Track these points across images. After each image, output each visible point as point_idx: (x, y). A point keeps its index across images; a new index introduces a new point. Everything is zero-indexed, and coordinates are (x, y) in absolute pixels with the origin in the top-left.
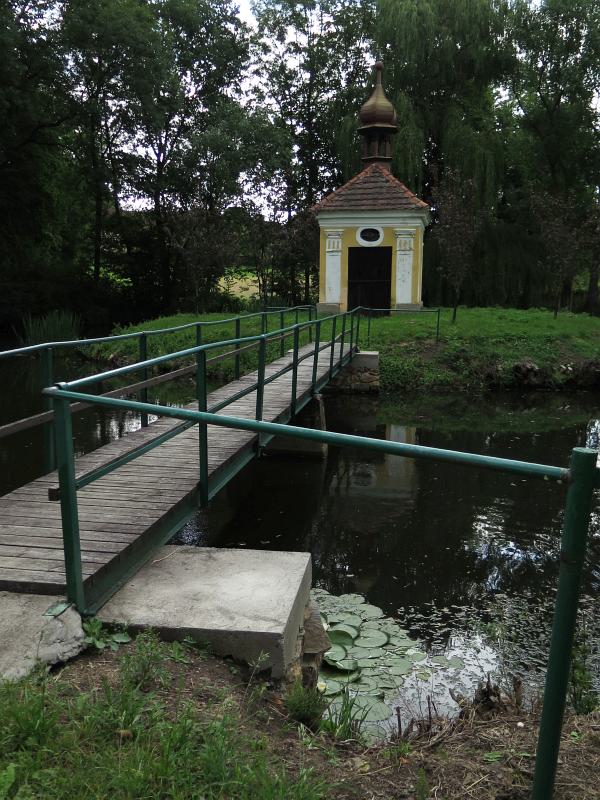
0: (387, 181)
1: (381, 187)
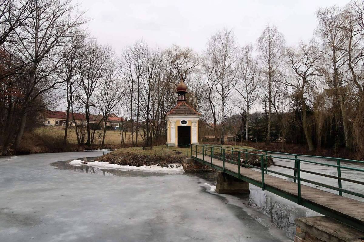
0: (187, 107)
1: (186, 109)
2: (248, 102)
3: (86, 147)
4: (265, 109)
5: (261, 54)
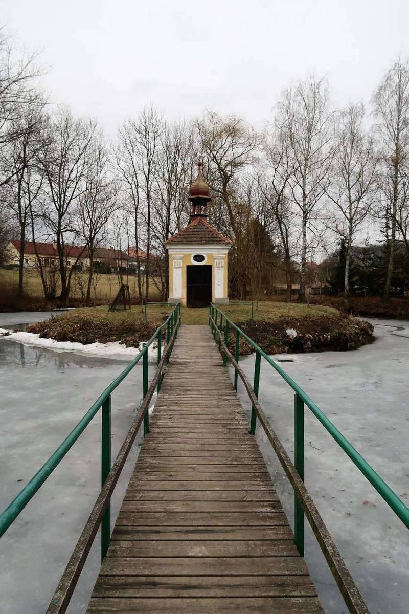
0: (207, 228)
2: (351, 220)
3: (58, 303)
4: (385, 234)
5: (380, 120)
